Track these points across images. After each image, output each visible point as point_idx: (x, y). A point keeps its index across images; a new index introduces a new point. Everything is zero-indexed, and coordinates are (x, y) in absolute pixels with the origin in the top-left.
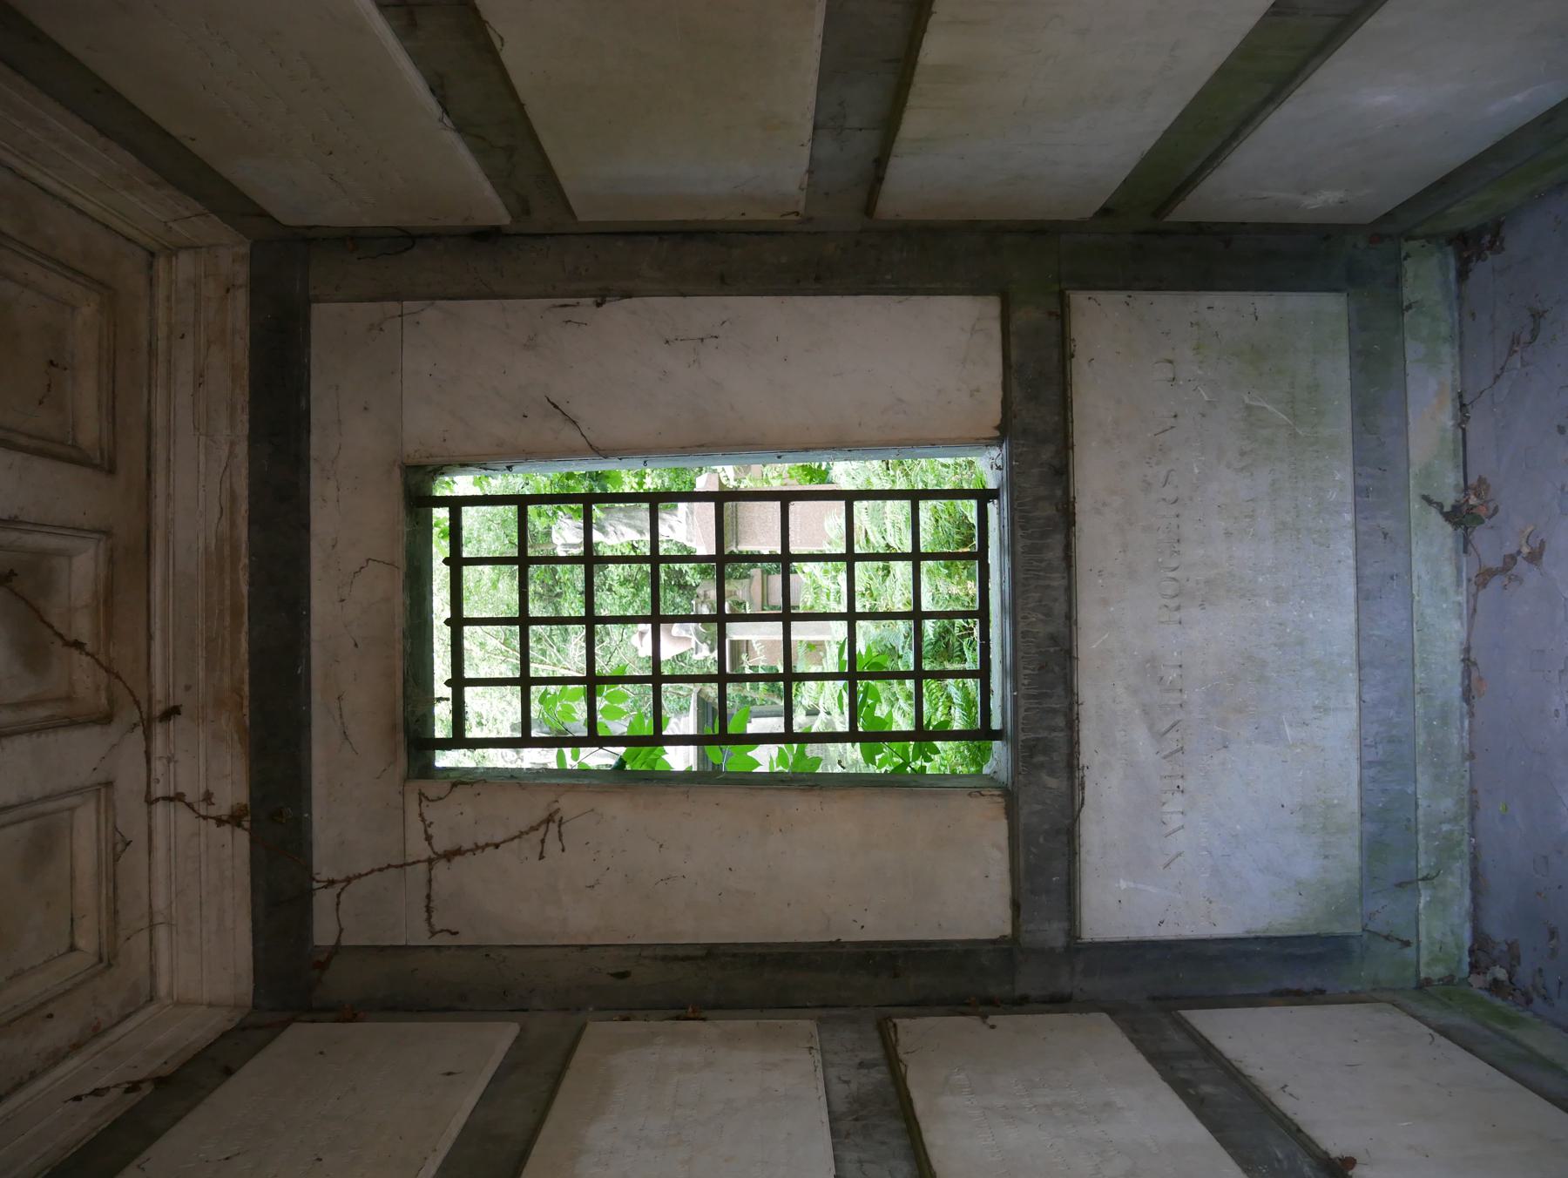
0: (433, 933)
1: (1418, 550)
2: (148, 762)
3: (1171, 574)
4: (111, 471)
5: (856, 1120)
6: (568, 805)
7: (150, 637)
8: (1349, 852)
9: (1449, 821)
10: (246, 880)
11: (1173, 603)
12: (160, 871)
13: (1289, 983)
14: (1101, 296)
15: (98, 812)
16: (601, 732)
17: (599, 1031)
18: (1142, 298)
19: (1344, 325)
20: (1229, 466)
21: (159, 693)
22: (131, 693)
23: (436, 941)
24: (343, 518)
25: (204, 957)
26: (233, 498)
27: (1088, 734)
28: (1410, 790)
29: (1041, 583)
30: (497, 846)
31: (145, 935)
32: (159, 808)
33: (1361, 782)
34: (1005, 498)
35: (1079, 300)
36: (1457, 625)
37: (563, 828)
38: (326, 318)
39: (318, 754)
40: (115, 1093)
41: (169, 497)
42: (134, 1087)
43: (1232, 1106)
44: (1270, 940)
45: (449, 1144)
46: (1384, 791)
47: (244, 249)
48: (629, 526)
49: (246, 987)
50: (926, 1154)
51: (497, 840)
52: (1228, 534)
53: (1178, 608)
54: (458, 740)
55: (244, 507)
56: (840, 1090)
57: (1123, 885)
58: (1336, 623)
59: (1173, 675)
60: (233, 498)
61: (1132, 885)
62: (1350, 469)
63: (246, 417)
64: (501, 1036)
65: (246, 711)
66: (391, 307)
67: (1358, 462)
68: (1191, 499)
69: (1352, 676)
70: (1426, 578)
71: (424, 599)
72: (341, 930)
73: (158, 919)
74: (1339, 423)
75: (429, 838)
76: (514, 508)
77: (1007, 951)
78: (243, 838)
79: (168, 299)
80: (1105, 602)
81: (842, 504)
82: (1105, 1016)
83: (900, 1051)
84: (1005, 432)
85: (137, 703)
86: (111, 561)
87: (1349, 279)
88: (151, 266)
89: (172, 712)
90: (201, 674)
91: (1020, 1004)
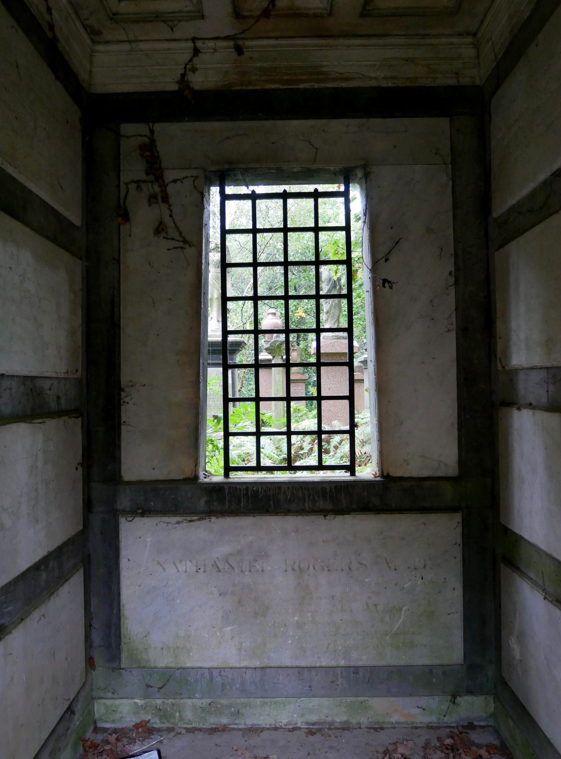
0: (126, 184)
1: (325, 701)
2: (214, 39)
3: (311, 566)
4: (363, 15)
5: (31, 390)
6: (190, 251)
7: (277, 38)
8: (164, 661)
9: (180, 716)
10: (153, 89)
11: (296, 567)
12: (157, 45)
13: (96, 624)
14: (459, 530)
15: (189, 12)
16: (229, 269)
17: (78, 266)
18: (458, 552)
19: (446, 662)
20: (369, 598)
21: (248, 43)
22: (249, 29)
23: (123, 187)
24: (340, 131)
25: (113, 69)
26: (348, 79)
27: (229, 521)
28: (197, 695)
29: (307, 497)
30: (171, 216)
31: (126, 39)
32: (190, 44)
33: (201, 668)
34: (352, 478)
35: (458, 517)
36: (285, 721)
37: (180, 249)
38: (441, 124)
39: (217, 125)
40: (48, 18)
41: (349, 46)
42: (51, 27)
43: (36, 584)
44: (119, 618)
45: (23, 181)
46: (196, 681)
47: (478, 82)
48: (331, 306)
49: (99, 90)
50: (16, 422)
51: (174, 215)
52: (333, 597)
53: (293, 569)
54: (224, 197)
55: (343, 85)
56: (46, 385)
57: (149, 540)
58: (284, 655)
59: (258, 567)
60: (348, 79)
61: (149, 544)
62: (367, 663)
63: (390, 85)
64: (74, 216)
65: (239, 88)
66: (449, 159)
67: (373, 669)
68: (351, 577)
69: (257, 664)
70: (310, 705)
71: (297, 180)
72: (128, 137)
73: (134, 45)
74: (392, 658)
75: (175, 181)
76: (344, 225)
77: (114, 478)
78: (174, 87)
79: (451, 44)
80: (297, 531)
81: (347, 394)
82: (81, 528)
83: (66, 418)
84: (387, 479)
85: (243, 32)
86: (315, 16)
87: (471, 667)
88: (468, 34)
89: (239, 50)
90: (258, 65)
91: (87, 480)
